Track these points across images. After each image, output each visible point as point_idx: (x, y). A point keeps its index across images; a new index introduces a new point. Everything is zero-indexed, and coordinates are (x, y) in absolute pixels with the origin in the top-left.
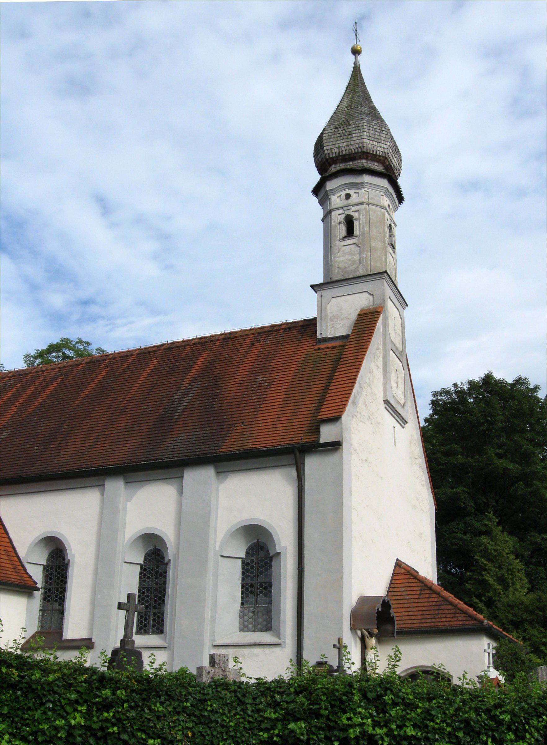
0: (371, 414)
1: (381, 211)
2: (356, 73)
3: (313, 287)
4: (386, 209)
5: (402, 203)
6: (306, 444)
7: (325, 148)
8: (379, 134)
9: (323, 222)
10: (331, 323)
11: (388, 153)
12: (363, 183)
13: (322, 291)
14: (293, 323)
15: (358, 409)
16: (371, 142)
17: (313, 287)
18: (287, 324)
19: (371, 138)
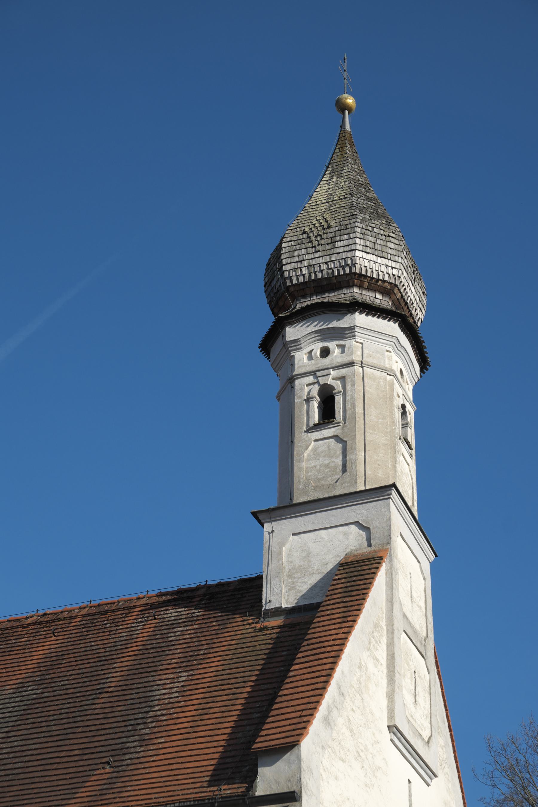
0: (362, 748)
1: (385, 380)
3: (255, 514)
4: (395, 376)
5: (427, 369)
7: (284, 268)
8: (382, 243)
9: (279, 400)
10: (290, 580)
11: (399, 277)
12: (352, 329)
13: (273, 523)
14: (221, 585)
15: (335, 735)
16: (369, 257)
17: (255, 514)
18: (208, 587)
19: (368, 250)
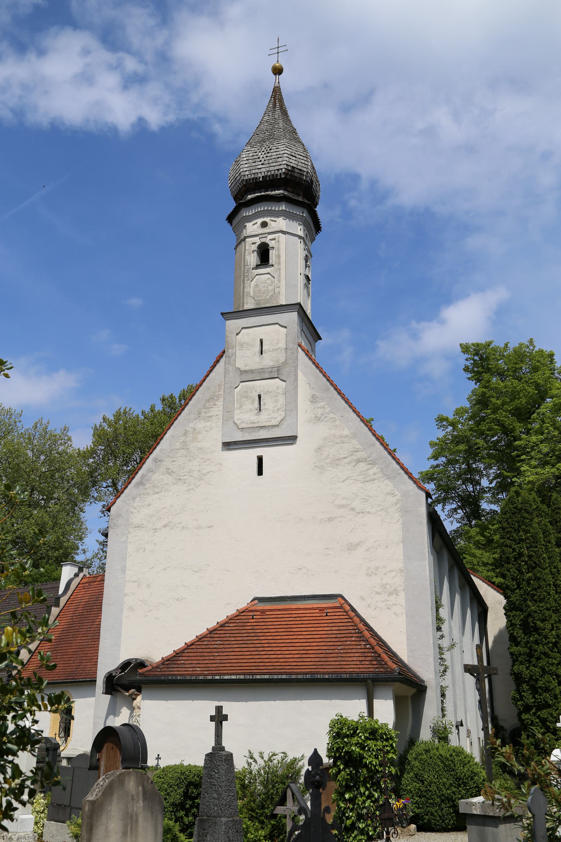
2: (277, 93)
3: (222, 314)
6: (243, 263)
17: (222, 314)
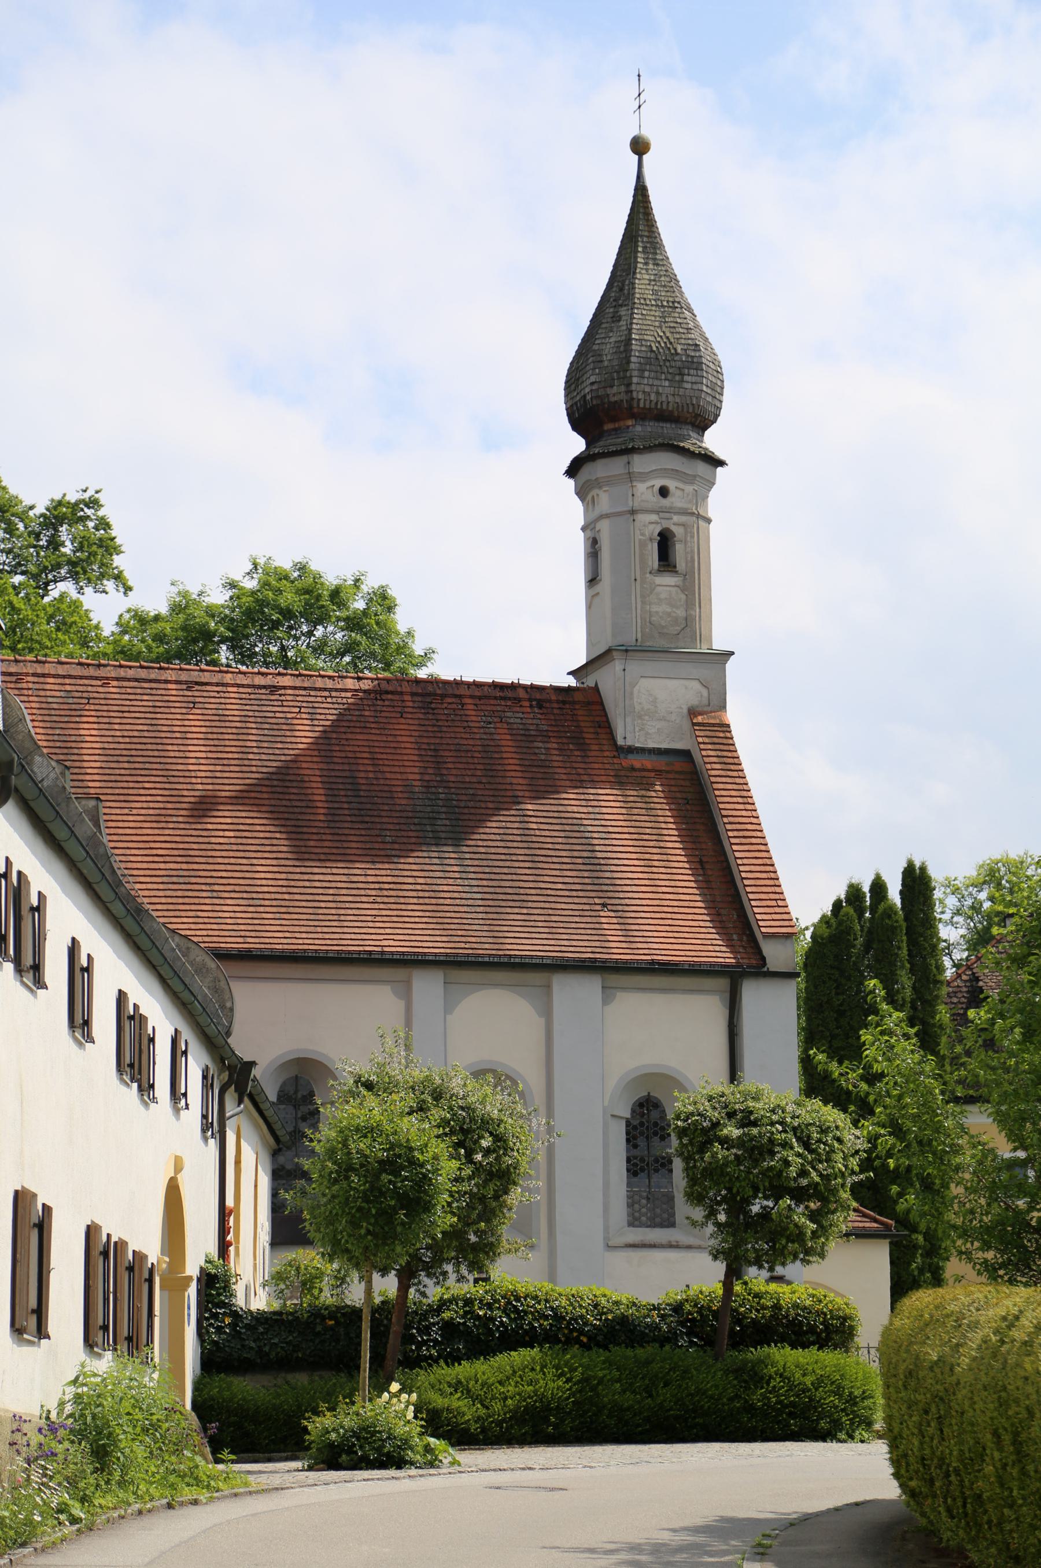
2: (641, 193)
